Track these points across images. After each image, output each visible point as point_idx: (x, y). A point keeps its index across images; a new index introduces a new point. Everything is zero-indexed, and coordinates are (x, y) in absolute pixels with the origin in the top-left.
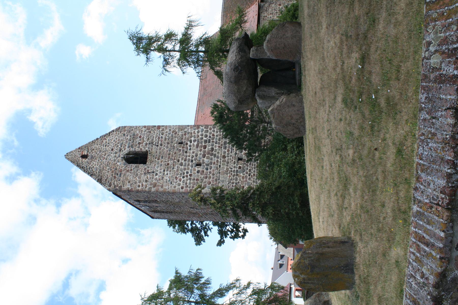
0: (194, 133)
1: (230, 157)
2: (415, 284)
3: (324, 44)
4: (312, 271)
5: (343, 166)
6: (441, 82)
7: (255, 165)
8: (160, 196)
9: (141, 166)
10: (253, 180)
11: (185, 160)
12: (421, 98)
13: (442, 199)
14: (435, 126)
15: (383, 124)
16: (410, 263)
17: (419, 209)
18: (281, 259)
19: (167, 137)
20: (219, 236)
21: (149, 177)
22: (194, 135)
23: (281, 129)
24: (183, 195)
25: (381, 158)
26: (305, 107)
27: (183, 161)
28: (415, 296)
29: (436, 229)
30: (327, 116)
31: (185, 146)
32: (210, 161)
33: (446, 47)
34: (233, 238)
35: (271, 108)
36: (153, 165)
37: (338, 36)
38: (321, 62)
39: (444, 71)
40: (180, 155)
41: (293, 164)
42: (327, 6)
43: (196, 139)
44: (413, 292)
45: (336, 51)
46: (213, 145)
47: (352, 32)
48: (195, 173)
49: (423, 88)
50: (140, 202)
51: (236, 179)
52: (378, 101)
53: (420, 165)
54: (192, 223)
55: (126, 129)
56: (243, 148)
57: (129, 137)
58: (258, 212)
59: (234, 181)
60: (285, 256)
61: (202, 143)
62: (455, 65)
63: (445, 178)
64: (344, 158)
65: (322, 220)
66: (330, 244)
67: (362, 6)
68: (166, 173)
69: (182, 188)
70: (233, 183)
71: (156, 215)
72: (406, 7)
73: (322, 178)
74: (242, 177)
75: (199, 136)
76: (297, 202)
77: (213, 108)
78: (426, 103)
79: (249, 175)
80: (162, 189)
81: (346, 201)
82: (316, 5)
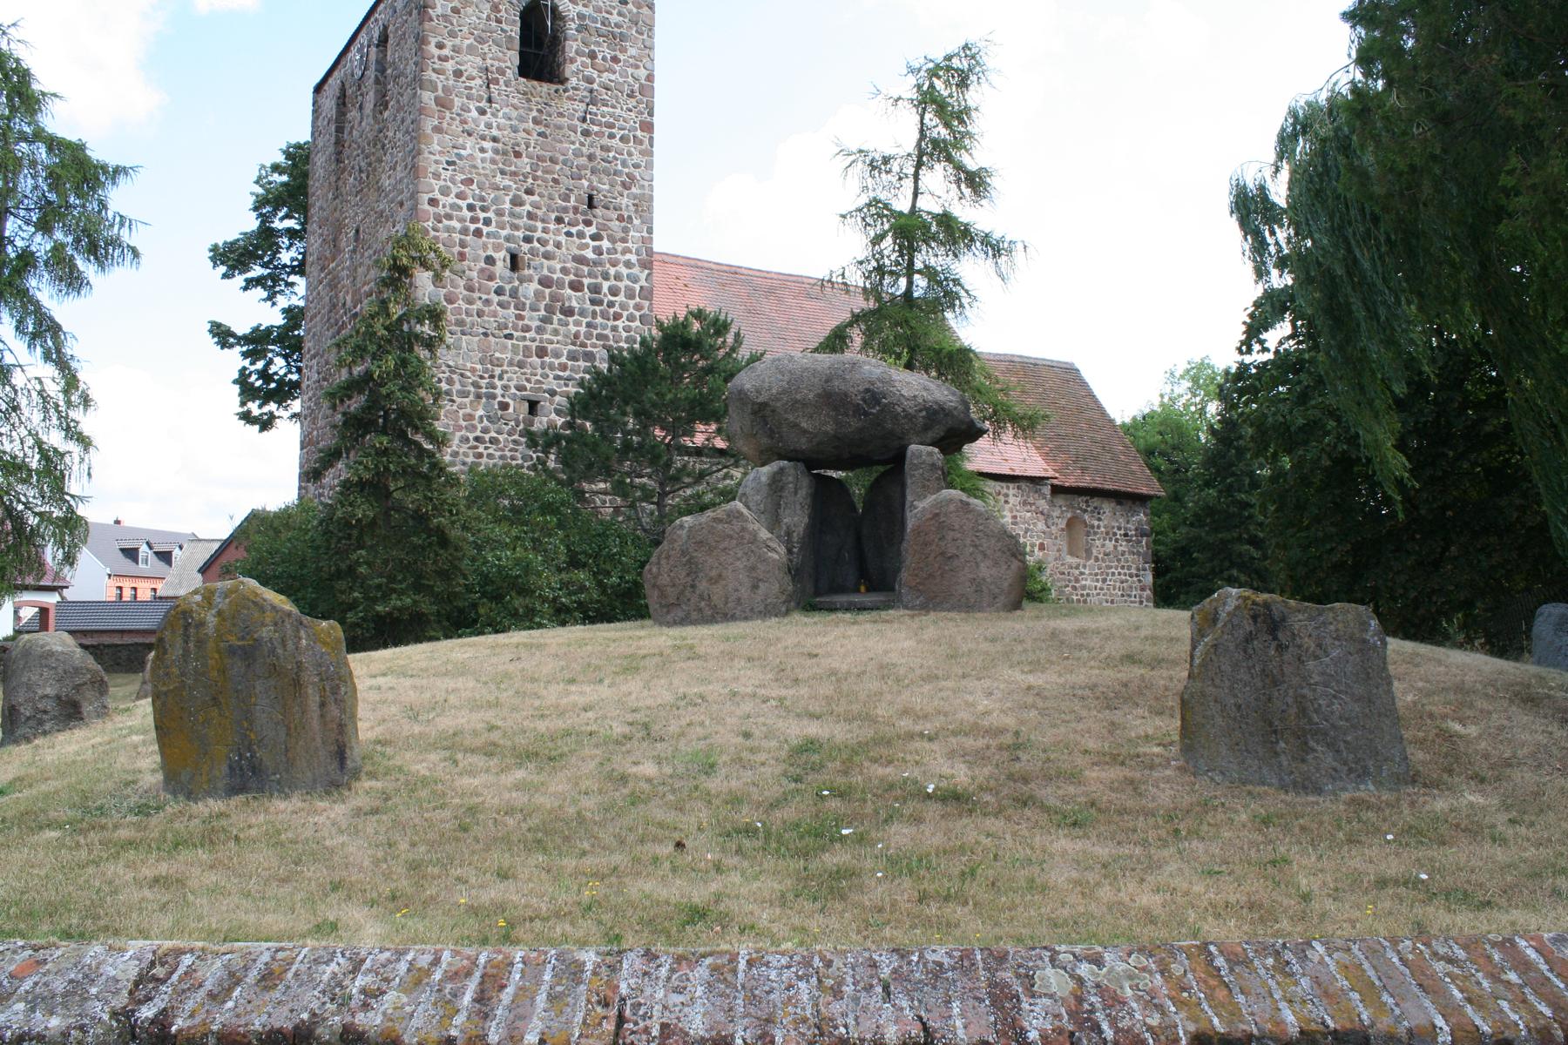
0: (626, 251)
1: (539, 371)
2: (335, 974)
3: (979, 679)
4: (232, 651)
5: (597, 746)
6: (996, 1002)
7: (513, 458)
8: (403, 122)
9: (513, 58)
10: (461, 451)
11: (530, 216)
12: (934, 951)
13: (647, 1030)
14: (864, 994)
15: (769, 863)
16: (400, 954)
17: (589, 967)
18: (157, 553)
19: (611, 154)
20: (248, 331)
21: (472, 84)
22: (619, 249)
23: (676, 545)
24: (408, 205)
25: (656, 860)
26: (750, 623)
27: (528, 207)
28: (290, 975)
29: (541, 1019)
30: (749, 690)
31: (580, 218)
32: (528, 302)
33: (1098, 1006)
34: (242, 380)
35: (745, 511)
36: (515, 101)
37: (1010, 721)
38: (918, 672)
39: (1031, 1005)
40: (551, 198)
41: (524, 591)
42: (1095, 686)
43: (605, 256)
44: (303, 968)
45: (964, 715)
46: (582, 313)
47: (1028, 762)
48: (485, 247)
49: (967, 955)
50: (378, 46)
51: (464, 394)
52: (838, 846)
53: (731, 961)
54: (291, 233)
55: (645, 10)
56: (573, 417)
57: (615, 18)
58: (357, 470)
59: (457, 386)
60: (167, 567)
61: (590, 275)
62: (1053, 1030)
63: (714, 1033)
64: (624, 749)
65: (384, 687)
66: (334, 711)
67: (1111, 789)
68: (488, 145)
69: (433, 202)
70: (450, 382)
71: (329, 104)
72: (1140, 908)
73: (533, 680)
74: (470, 415)
75: (614, 266)
76: (395, 602)
77: (717, 320)
78: (925, 965)
79: (477, 439)
80: (429, 131)
81: (478, 760)
82: (1093, 653)
